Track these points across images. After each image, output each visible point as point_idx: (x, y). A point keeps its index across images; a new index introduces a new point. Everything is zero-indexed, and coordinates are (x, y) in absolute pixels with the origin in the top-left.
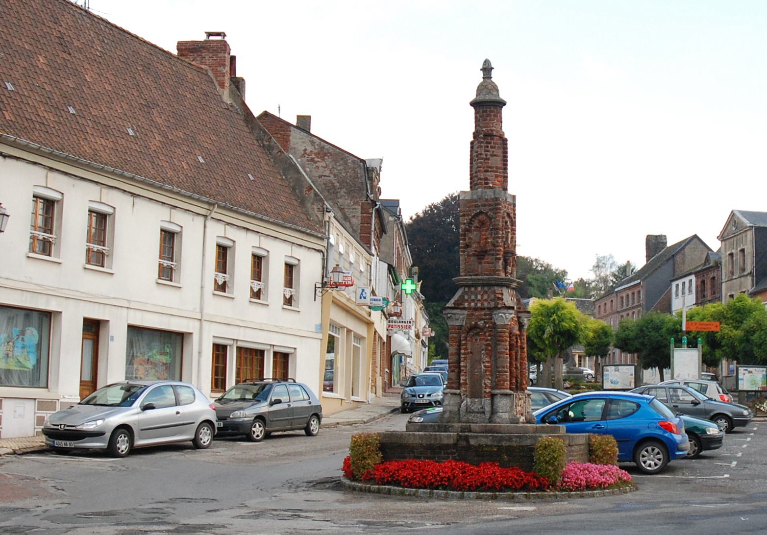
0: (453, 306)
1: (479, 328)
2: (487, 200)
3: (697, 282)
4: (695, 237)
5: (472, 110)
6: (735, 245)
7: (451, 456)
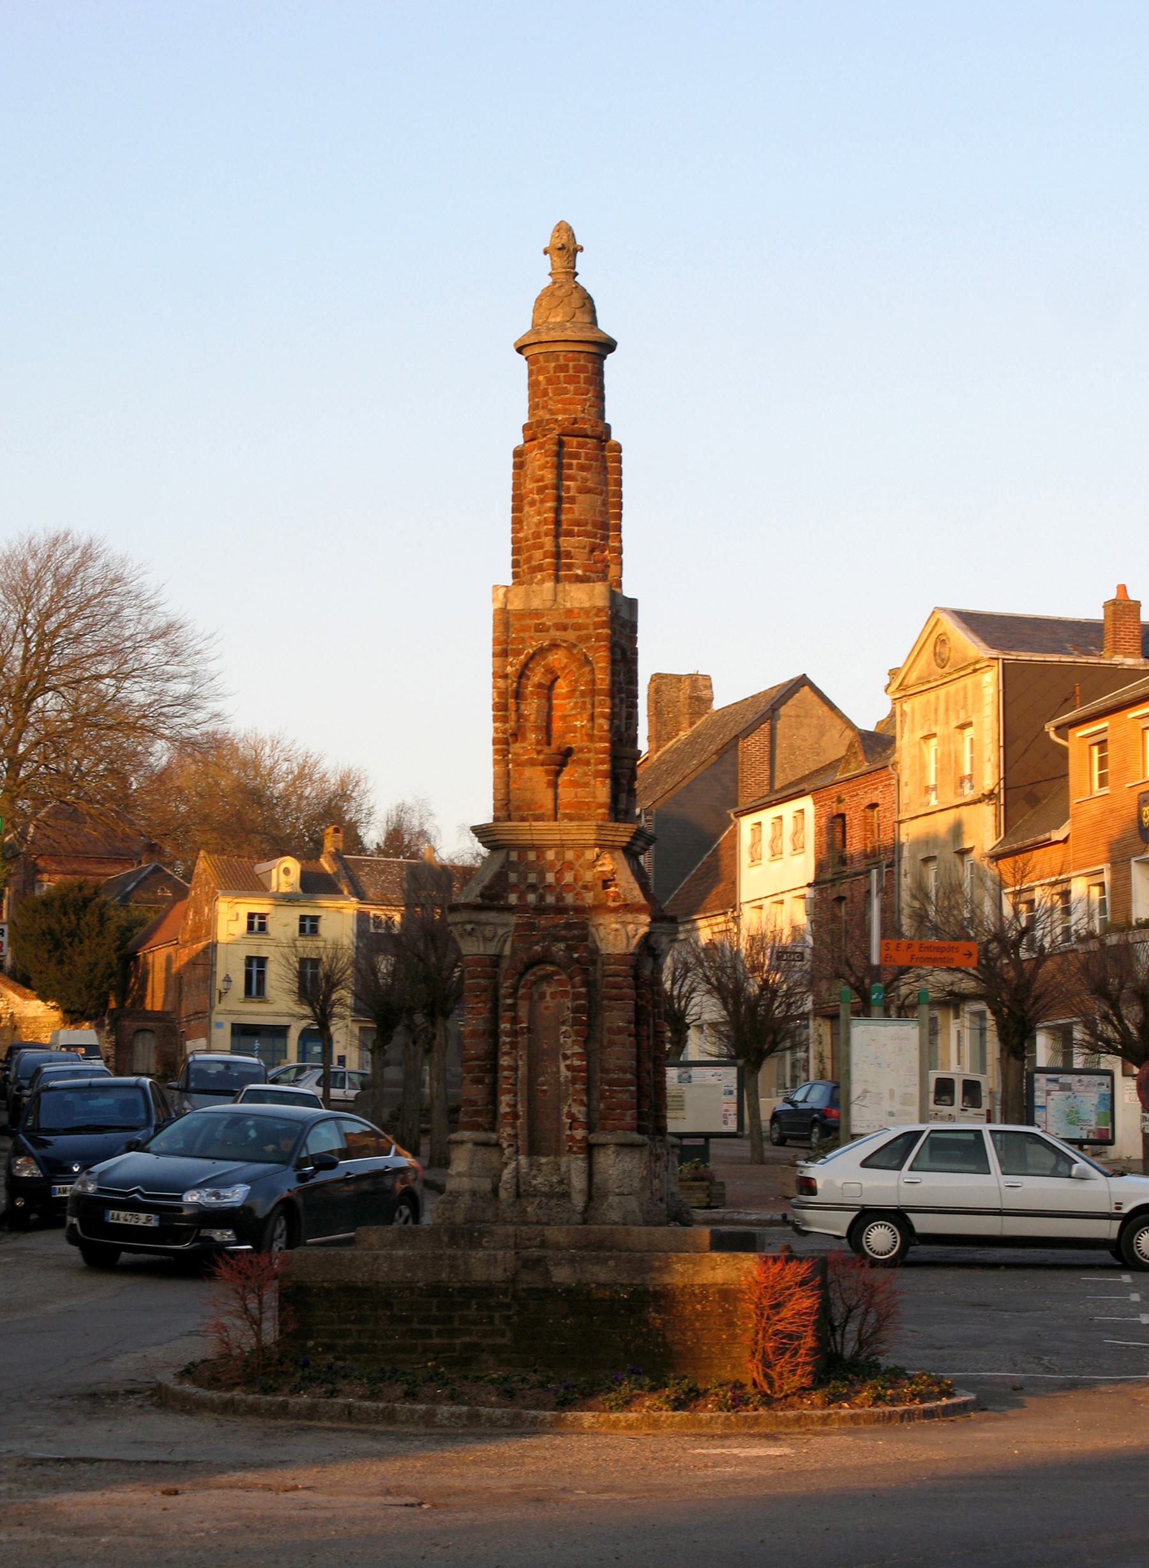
0: (479, 900)
1: (552, 963)
2: (569, 612)
3: (818, 816)
4: (803, 682)
5: (521, 364)
6: (941, 710)
7: (497, 1315)
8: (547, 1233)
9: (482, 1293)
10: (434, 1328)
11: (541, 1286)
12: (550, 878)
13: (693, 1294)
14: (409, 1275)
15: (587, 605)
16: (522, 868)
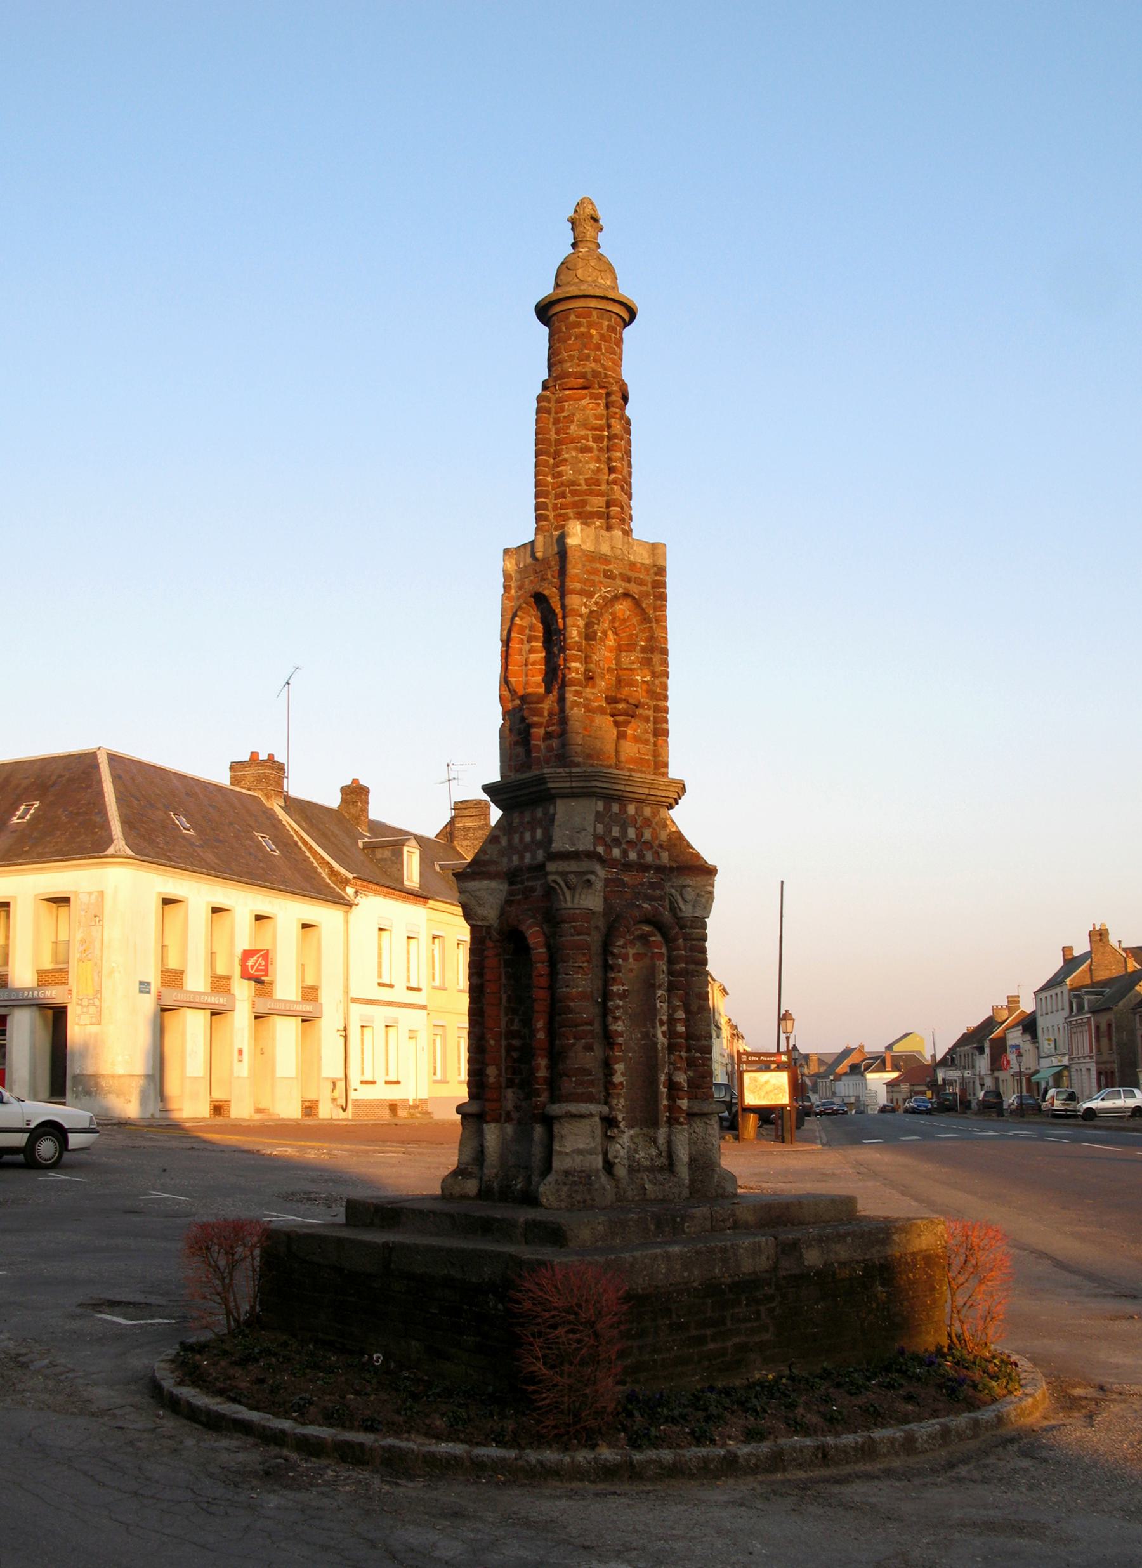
7: (762, 1308)
8: (738, 1213)
9: (747, 1286)
10: (709, 1332)
11: (796, 1271)
12: (631, 833)
13: (907, 1263)
14: (686, 1274)
15: (647, 562)
16: (607, 820)
